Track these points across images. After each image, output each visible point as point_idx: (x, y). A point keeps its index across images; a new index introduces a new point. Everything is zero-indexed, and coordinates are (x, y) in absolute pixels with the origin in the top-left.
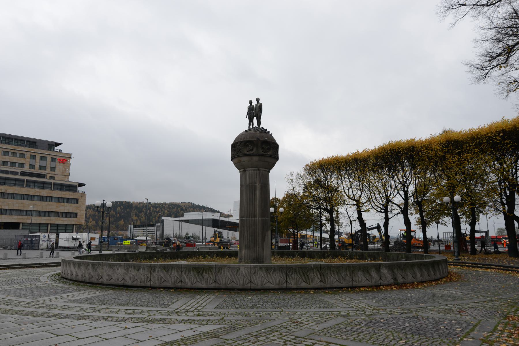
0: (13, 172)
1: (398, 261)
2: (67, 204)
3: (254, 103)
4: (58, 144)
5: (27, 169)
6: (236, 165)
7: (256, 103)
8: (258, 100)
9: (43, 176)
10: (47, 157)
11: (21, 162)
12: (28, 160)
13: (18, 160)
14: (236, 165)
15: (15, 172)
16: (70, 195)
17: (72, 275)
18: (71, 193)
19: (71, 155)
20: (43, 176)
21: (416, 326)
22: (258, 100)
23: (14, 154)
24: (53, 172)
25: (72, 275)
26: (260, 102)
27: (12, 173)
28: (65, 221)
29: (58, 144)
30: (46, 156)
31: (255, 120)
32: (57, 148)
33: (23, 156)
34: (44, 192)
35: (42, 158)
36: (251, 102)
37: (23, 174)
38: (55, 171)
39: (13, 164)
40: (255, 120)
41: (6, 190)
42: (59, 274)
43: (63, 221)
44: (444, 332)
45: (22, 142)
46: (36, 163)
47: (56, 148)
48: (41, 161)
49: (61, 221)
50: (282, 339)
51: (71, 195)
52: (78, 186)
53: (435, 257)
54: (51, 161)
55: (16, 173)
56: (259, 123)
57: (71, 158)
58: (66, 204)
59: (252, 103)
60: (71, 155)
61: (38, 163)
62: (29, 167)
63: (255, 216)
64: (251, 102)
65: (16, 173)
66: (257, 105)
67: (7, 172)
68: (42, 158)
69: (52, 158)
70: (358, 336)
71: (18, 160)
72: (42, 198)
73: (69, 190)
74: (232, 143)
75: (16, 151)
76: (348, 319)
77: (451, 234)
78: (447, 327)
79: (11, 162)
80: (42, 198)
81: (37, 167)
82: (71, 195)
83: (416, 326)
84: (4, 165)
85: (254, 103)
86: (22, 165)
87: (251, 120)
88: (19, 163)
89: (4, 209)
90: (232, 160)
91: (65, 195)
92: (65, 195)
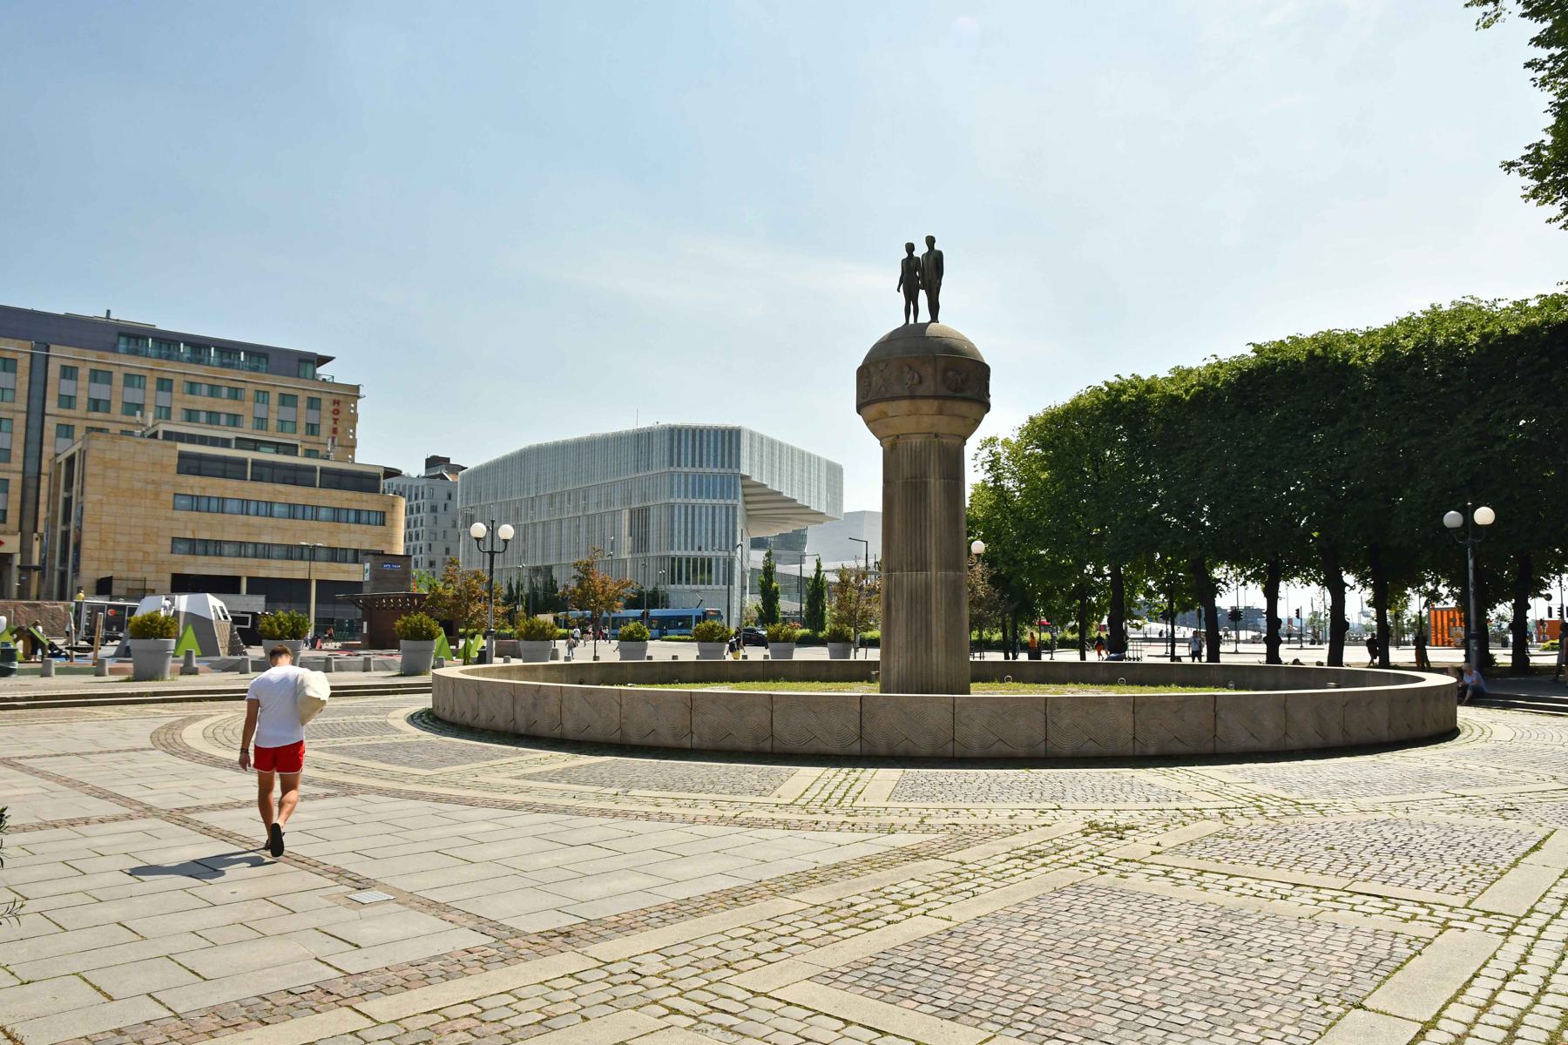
0: (217, 438)
1: (1135, 701)
2: (357, 527)
3: (921, 251)
4: (325, 360)
5: (247, 431)
6: (871, 424)
7: (926, 250)
8: (931, 241)
9: (291, 449)
10: (111, 373)
11: (231, 411)
12: (249, 404)
13: (224, 405)
14: (871, 424)
15: (223, 439)
16: (362, 501)
17: (453, 712)
18: (366, 496)
19: (357, 388)
20: (291, 449)
21: (1399, 839)
22: (931, 241)
23: (214, 391)
24: (313, 439)
25: (453, 712)
26: (937, 247)
27: (214, 442)
28: (354, 572)
29: (325, 360)
30: (143, 373)
31: (923, 297)
32: (323, 371)
33: (235, 394)
34: (298, 494)
35: (129, 380)
36: (910, 248)
37: (242, 443)
38: (108, 411)
39: (213, 418)
40: (923, 297)
41: (204, 488)
42: (428, 712)
43: (348, 572)
44: (1469, 852)
45: (140, 342)
46: (270, 414)
47: (319, 370)
48: (94, 385)
49: (344, 572)
50: (665, 977)
51: (366, 502)
52: (382, 475)
53: (1423, 680)
54: (157, 390)
55: (225, 443)
56: (934, 308)
57: (359, 397)
58: (354, 527)
59: (913, 249)
60: (357, 388)
61: (275, 411)
62: (56, 404)
63: (924, 567)
64: (910, 248)
65: (225, 443)
66: (927, 255)
67: (203, 440)
68: (95, 376)
69: (64, 368)
70: (1266, 859)
71: (224, 405)
72: (293, 511)
73: (361, 489)
74: (859, 363)
75: (218, 383)
76: (640, 982)
77: (1451, 613)
78: (1472, 842)
79: (207, 412)
80: (293, 511)
81: (273, 423)
82: (366, 502)
83: (1399, 839)
84: (189, 421)
85: (921, 251)
86: (234, 420)
87: (911, 298)
88: (228, 415)
89: (200, 540)
90: (859, 412)
91: (351, 500)
92: (351, 500)
